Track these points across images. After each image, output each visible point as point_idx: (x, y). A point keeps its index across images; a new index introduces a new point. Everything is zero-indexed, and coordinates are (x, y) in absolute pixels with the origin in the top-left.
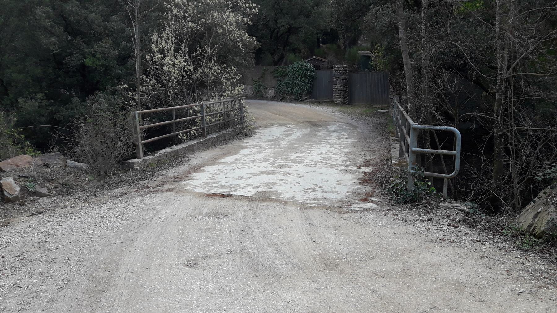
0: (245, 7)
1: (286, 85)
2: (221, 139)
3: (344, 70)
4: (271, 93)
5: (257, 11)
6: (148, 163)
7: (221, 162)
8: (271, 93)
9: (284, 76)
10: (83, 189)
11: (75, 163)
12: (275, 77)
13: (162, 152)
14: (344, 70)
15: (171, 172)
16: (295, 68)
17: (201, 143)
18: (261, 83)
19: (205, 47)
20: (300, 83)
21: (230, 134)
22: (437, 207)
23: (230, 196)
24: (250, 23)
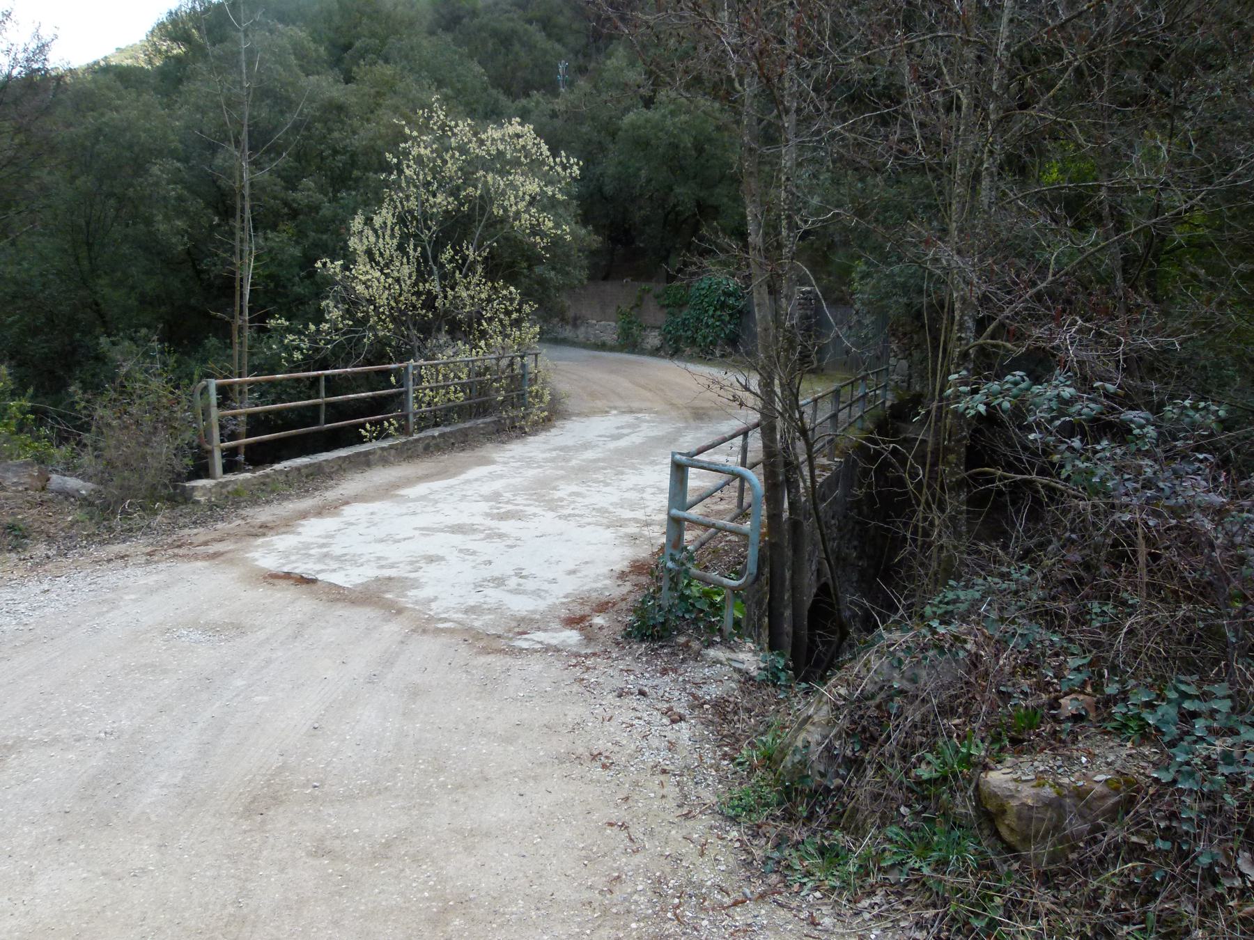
0: (552, 164)
1: (683, 324)
2: (452, 441)
3: (806, 299)
4: (653, 339)
5: (578, 172)
6: (230, 488)
7: (397, 496)
8: (653, 339)
9: (681, 304)
10: (50, 539)
11: (65, 482)
12: (663, 306)
13: (277, 467)
14: (806, 299)
15: (263, 514)
16: (703, 289)
17: (391, 447)
18: (633, 318)
19: (461, 247)
20: (710, 321)
21: (482, 429)
22: (697, 656)
23: (313, 581)
24: (559, 196)
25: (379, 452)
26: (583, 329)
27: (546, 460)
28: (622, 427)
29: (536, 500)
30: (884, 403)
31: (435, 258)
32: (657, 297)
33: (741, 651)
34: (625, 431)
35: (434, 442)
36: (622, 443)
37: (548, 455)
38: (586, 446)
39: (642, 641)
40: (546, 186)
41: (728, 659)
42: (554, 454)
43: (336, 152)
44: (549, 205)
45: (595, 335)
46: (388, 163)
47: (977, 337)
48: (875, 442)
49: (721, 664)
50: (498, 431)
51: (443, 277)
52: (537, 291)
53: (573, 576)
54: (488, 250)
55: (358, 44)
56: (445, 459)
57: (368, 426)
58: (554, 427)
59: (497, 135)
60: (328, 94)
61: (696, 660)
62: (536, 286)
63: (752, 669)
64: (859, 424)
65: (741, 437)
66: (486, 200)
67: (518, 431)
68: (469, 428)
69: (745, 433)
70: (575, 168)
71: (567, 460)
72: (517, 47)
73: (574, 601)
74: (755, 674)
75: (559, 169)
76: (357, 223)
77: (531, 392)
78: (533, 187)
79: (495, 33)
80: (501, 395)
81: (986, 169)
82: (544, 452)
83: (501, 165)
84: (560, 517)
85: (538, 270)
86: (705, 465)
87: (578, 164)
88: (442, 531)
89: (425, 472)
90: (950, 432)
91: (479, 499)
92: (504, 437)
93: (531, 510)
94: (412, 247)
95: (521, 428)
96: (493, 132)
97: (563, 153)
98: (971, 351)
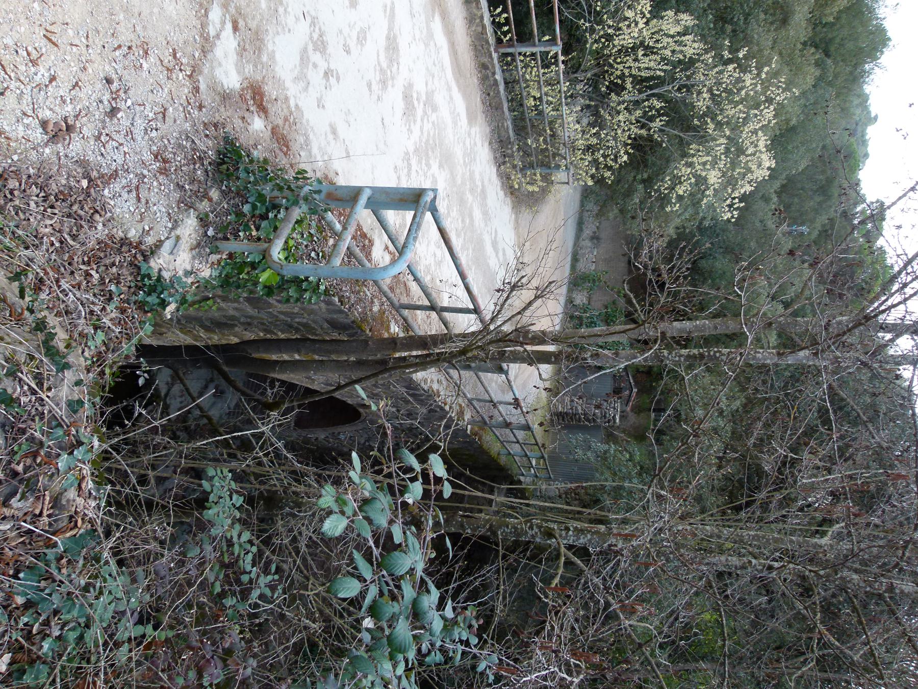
2: (492, 94)
5: (725, 218)
8: (580, 298)
17: (484, 27)
18: (597, 284)
19: (663, 115)
25: (479, 14)
26: (589, 244)
27: (472, 173)
28: (504, 254)
29: (428, 140)
30: (523, 475)
31: (653, 95)
32: (614, 303)
33: (194, 258)
34: (501, 254)
35: (490, 74)
36: (489, 249)
37: (477, 177)
38: (485, 214)
39: (219, 153)
40: (714, 189)
41: (178, 238)
42: (479, 183)
43: (747, 16)
44: (695, 199)
45: (584, 254)
46: (738, 50)
47: (570, 547)
48: (447, 427)
49: (173, 229)
50: (501, 141)
51: (637, 103)
52: (622, 187)
53: (328, 129)
54: (659, 139)
55: (829, 62)
56: (474, 81)
57: (505, 15)
58: (506, 195)
59: (761, 144)
60: (797, 9)
61: (179, 202)
62: (626, 186)
63: (161, 261)
64: (503, 451)
65: (471, 307)
66: (703, 138)
67: (501, 160)
68: (503, 112)
69: (476, 311)
70: (729, 215)
71: (472, 190)
72: (818, 199)
73: (291, 113)
74: (152, 263)
75: (728, 202)
76: (687, 19)
77: (535, 174)
78: (713, 177)
79: (830, 181)
80: (532, 142)
81: (750, 562)
82: (481, 174)
83: (736, 150)
84: (407, 153)
85: (640, 187)
86: (417, 219)
87: (732, 217)
88: (390, 29)
89: (459, 53)
90: (471, 517)
91: (429, 87)
92: (496, 146)
93: (416, 129)
94: (665, 67)
95: (504, 163)
96: (763, 141)
97: (742, 205)
98: (554, 540)
